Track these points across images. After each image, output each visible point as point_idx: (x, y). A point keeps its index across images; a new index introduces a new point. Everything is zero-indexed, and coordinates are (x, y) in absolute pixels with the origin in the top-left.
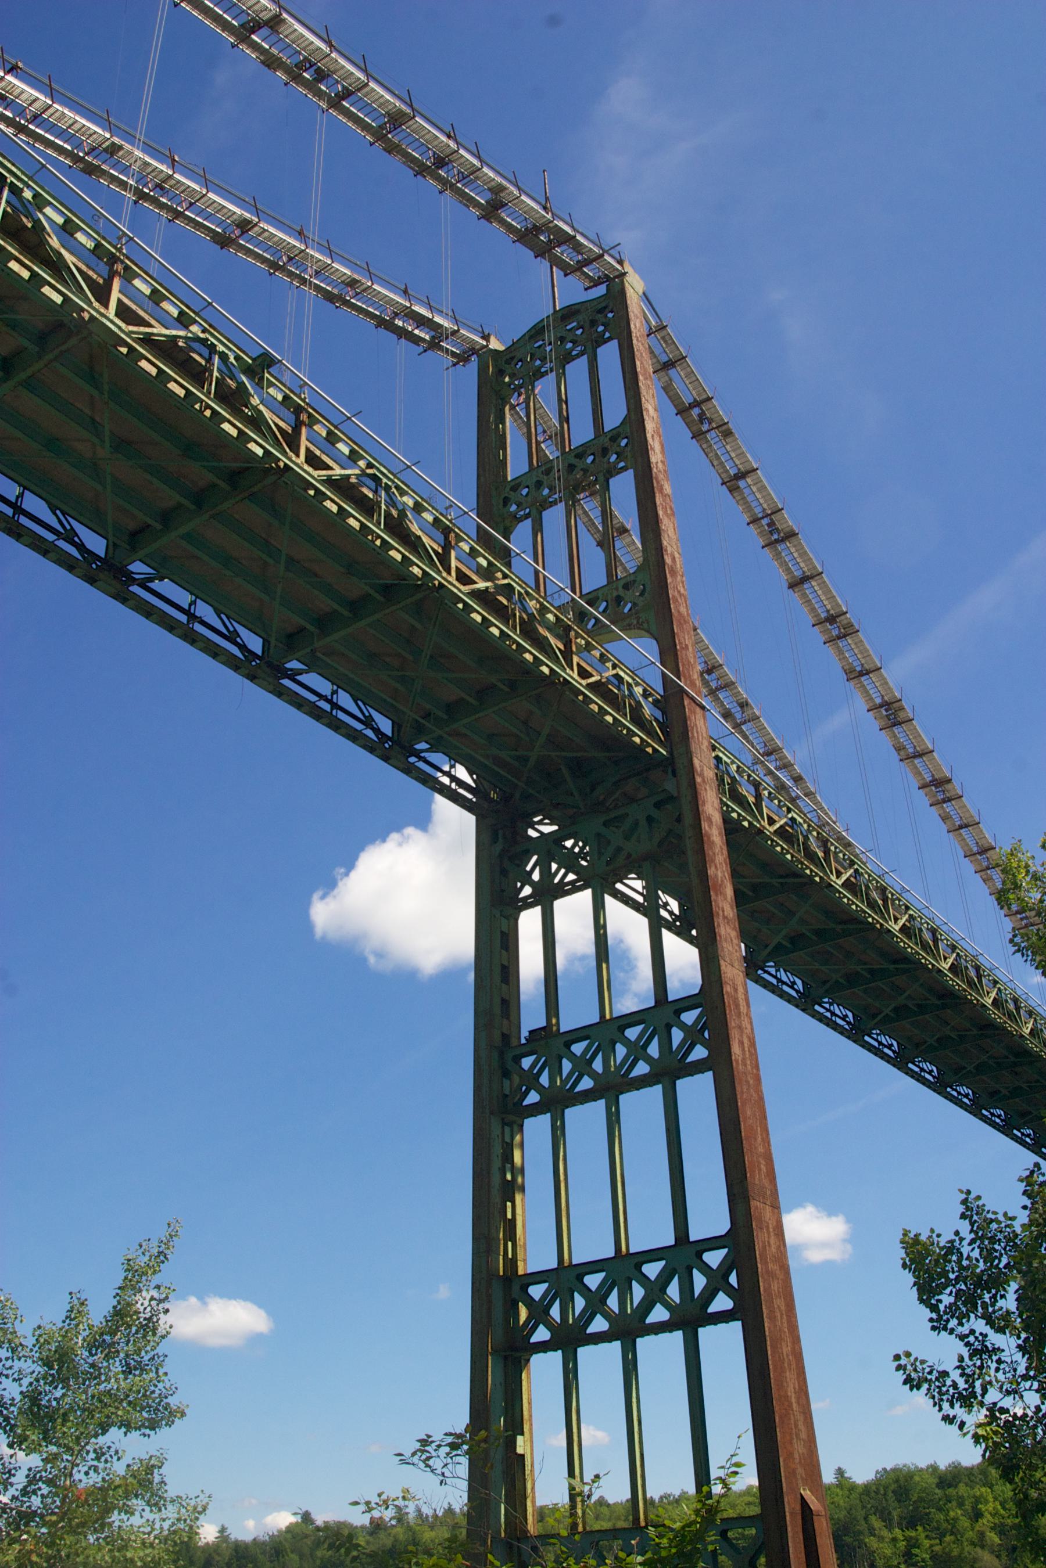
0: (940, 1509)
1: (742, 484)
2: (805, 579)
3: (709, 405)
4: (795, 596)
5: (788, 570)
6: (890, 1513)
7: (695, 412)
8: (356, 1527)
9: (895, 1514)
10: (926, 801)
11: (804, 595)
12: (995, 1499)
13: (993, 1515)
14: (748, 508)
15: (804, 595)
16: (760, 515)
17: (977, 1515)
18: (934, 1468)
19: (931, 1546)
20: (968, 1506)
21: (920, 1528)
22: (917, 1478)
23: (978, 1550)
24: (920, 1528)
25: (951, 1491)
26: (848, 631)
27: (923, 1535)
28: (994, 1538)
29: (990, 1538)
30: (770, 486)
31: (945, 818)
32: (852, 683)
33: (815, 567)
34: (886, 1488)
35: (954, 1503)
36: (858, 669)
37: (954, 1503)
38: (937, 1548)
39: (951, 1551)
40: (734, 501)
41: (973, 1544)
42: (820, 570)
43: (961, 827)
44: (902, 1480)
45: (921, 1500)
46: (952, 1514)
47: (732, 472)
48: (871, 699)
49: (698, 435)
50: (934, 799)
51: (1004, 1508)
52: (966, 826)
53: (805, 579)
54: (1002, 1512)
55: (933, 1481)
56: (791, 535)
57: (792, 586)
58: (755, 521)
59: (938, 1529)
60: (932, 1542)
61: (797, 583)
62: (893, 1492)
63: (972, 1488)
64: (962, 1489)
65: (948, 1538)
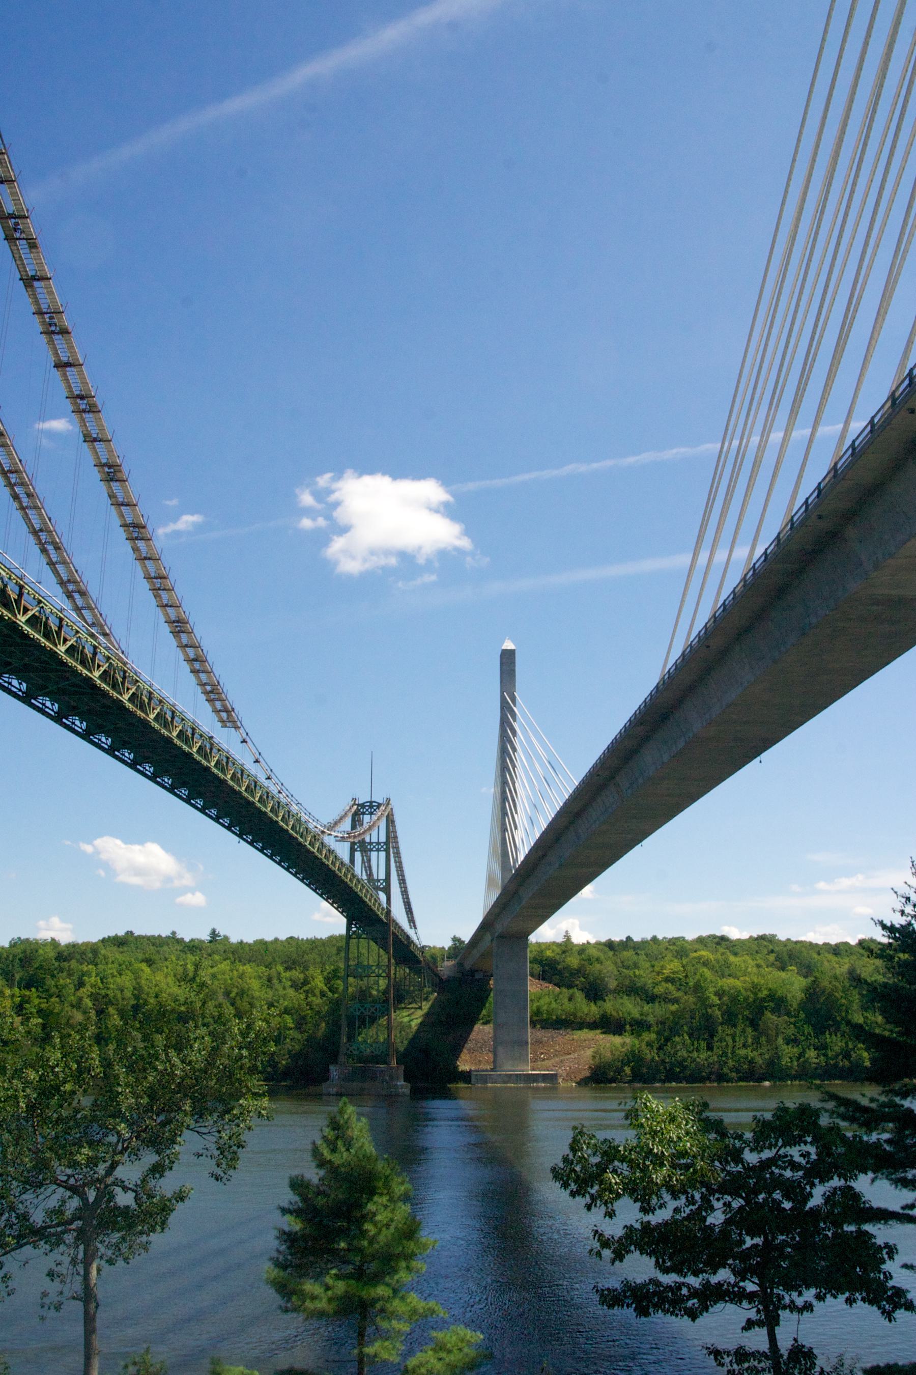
0: (53, 976)
1: (36, 284)
2: (68, 365)
3: (24, 221)
4: (56, 374)
5: (56, 354)
6: (13, 975)
7: (11, 222)
8: (95, 944)
9: (17, 977)
10: (124, 536)
11: (65, 375)
12: (97, 975)
13: (93, 986)
14: (36, 302)
15: (65, 375)
16: (45, 310)
17: (81, 984)
18: (54, 943)
19: (40, 1003)
20: (75, 977)
21: (33, 990)
22: (41, 951)
23: (75, 1010)
24: (33, 990)
25: (65, 964)
26: (93, 409)
27: (35, 995)
28: (88, 1002)
29: (86, 1004)
30: (58, 293)
31: (135, 549)
32: (86, 444)
33: (78, 359)
34: (15, 956)
35: (65, 974)
36: (95, 436)
37: (65, 974)
38: (43, 1006)
39: (54, 1009)
40: (27, 294)
41: (73, 1006)
42: (81, 362)
43: (145, 558)
44: (28, 952)
45: (41, 967)
46: (61, 981)
47: (30, 274)
48: (98, 458)
49: (9, 239)
50: (130, 536)
51: (102, 982)
52: (149, 559)
53: (68, 365)
54: (101, 985)
55: (52, 954)
56: (64, 332)
57: (56, 366)
58: (40, 313)
59: (47, 991)
60: (42, 1000)
61: (61, 365)
62: (557, 1174)
63: (81, 964)
64: (73, 964)
65: (53, 999)
